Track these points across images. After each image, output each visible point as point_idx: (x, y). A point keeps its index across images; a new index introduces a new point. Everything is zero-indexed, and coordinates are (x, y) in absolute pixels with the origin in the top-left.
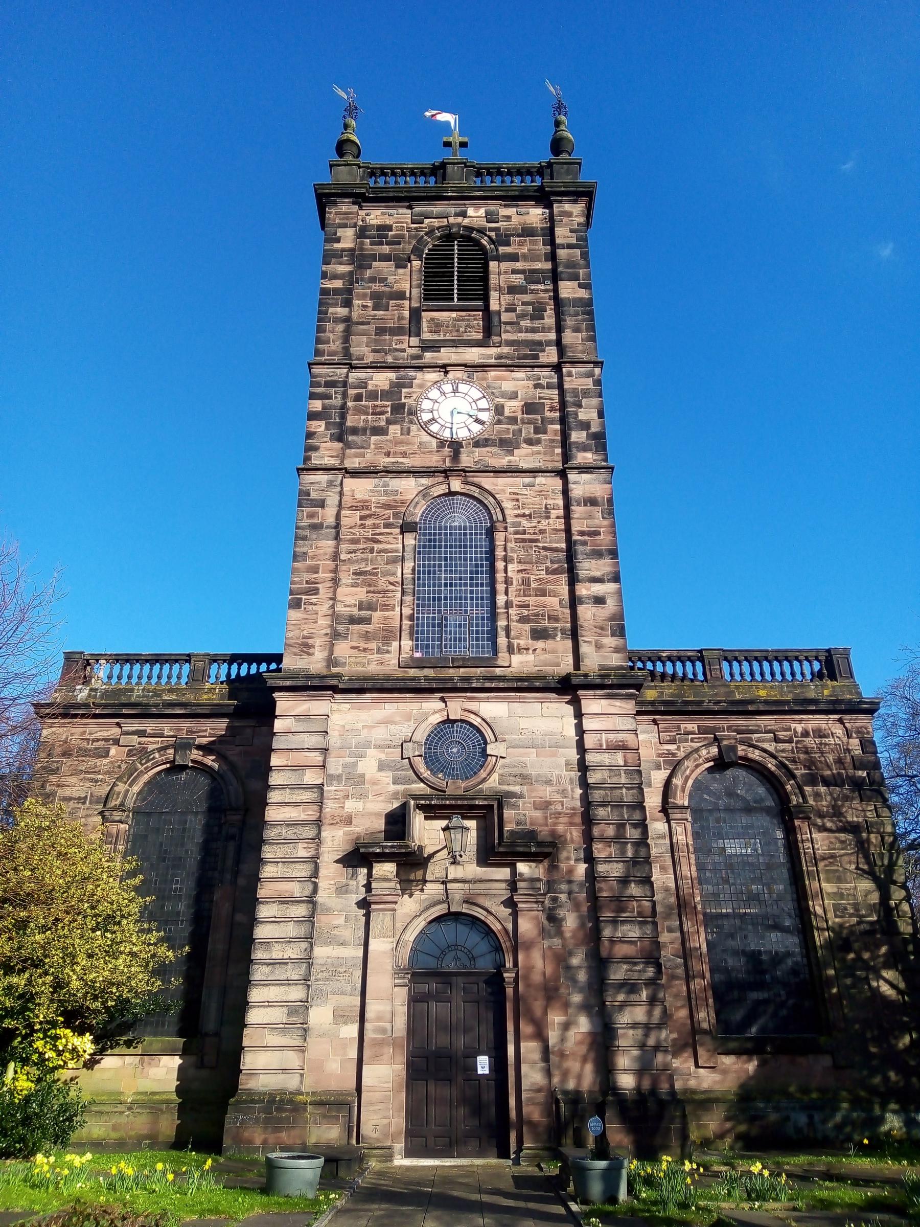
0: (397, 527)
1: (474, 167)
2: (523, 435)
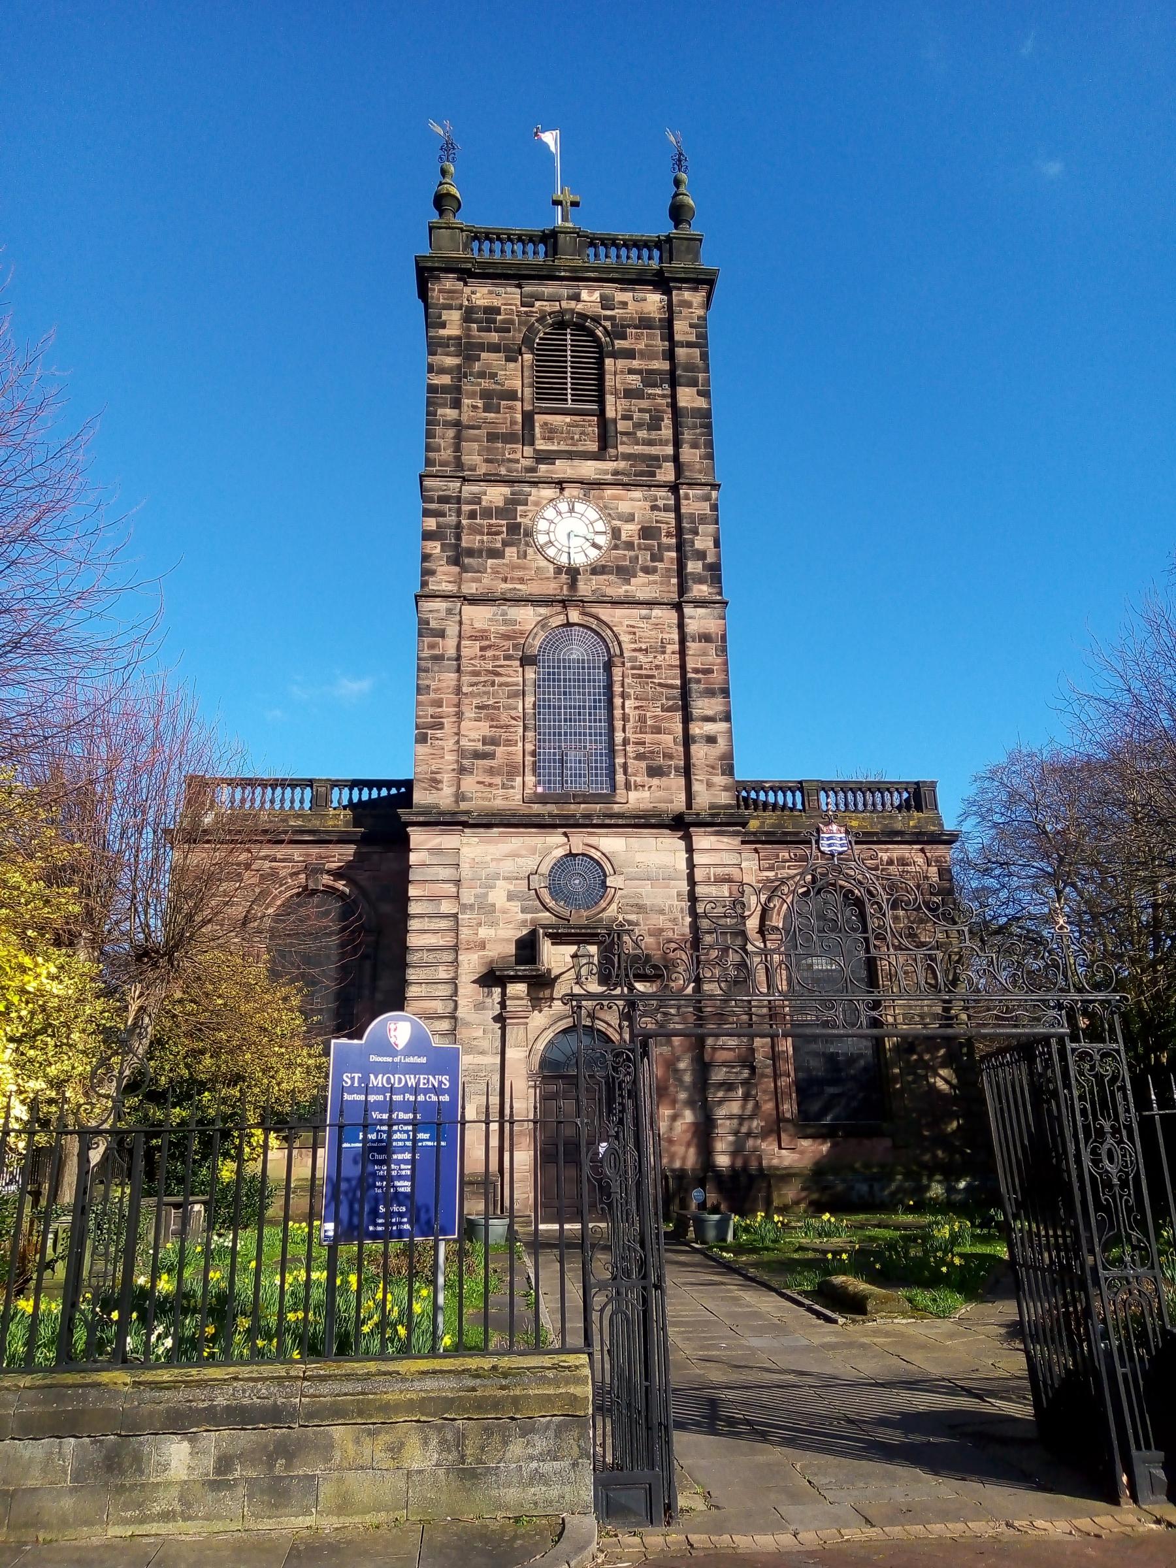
0: (516, 659)
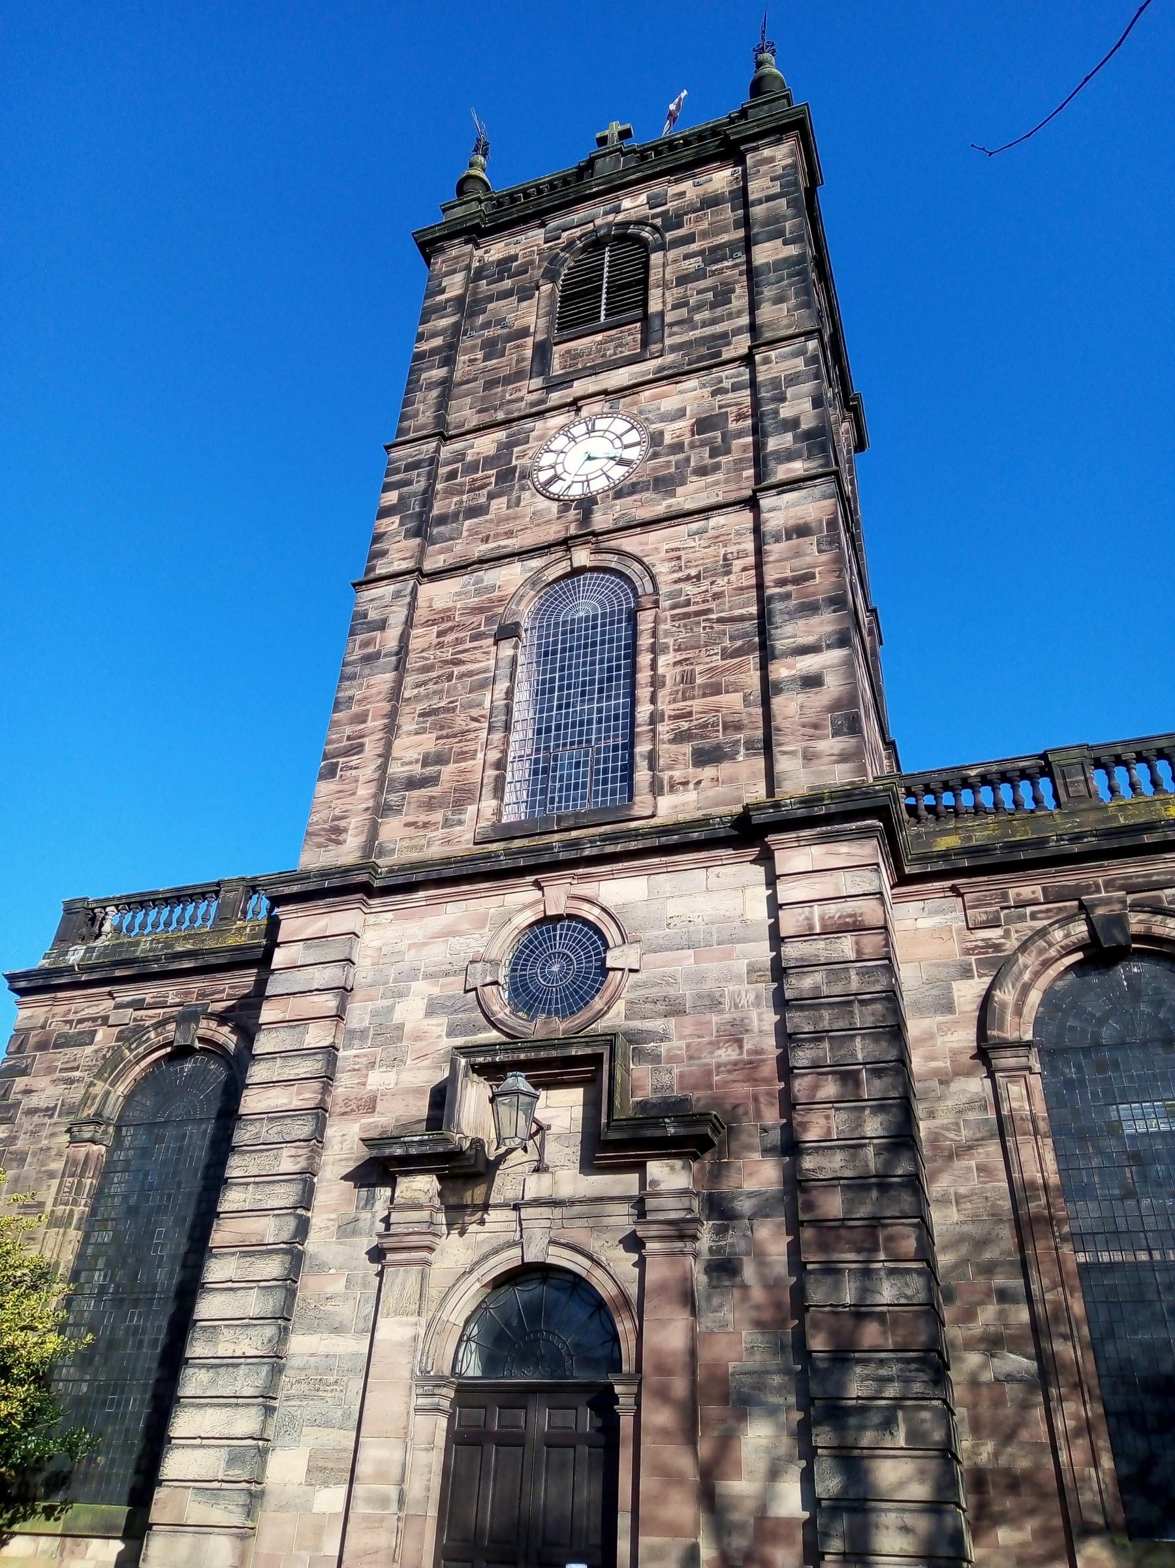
0: (490, 636)
1: (634, 151)
2: (692, 464)
